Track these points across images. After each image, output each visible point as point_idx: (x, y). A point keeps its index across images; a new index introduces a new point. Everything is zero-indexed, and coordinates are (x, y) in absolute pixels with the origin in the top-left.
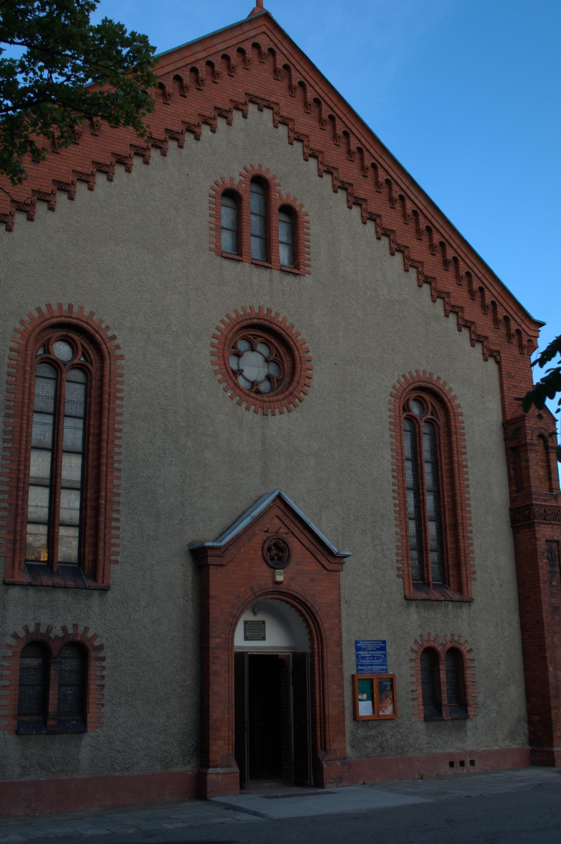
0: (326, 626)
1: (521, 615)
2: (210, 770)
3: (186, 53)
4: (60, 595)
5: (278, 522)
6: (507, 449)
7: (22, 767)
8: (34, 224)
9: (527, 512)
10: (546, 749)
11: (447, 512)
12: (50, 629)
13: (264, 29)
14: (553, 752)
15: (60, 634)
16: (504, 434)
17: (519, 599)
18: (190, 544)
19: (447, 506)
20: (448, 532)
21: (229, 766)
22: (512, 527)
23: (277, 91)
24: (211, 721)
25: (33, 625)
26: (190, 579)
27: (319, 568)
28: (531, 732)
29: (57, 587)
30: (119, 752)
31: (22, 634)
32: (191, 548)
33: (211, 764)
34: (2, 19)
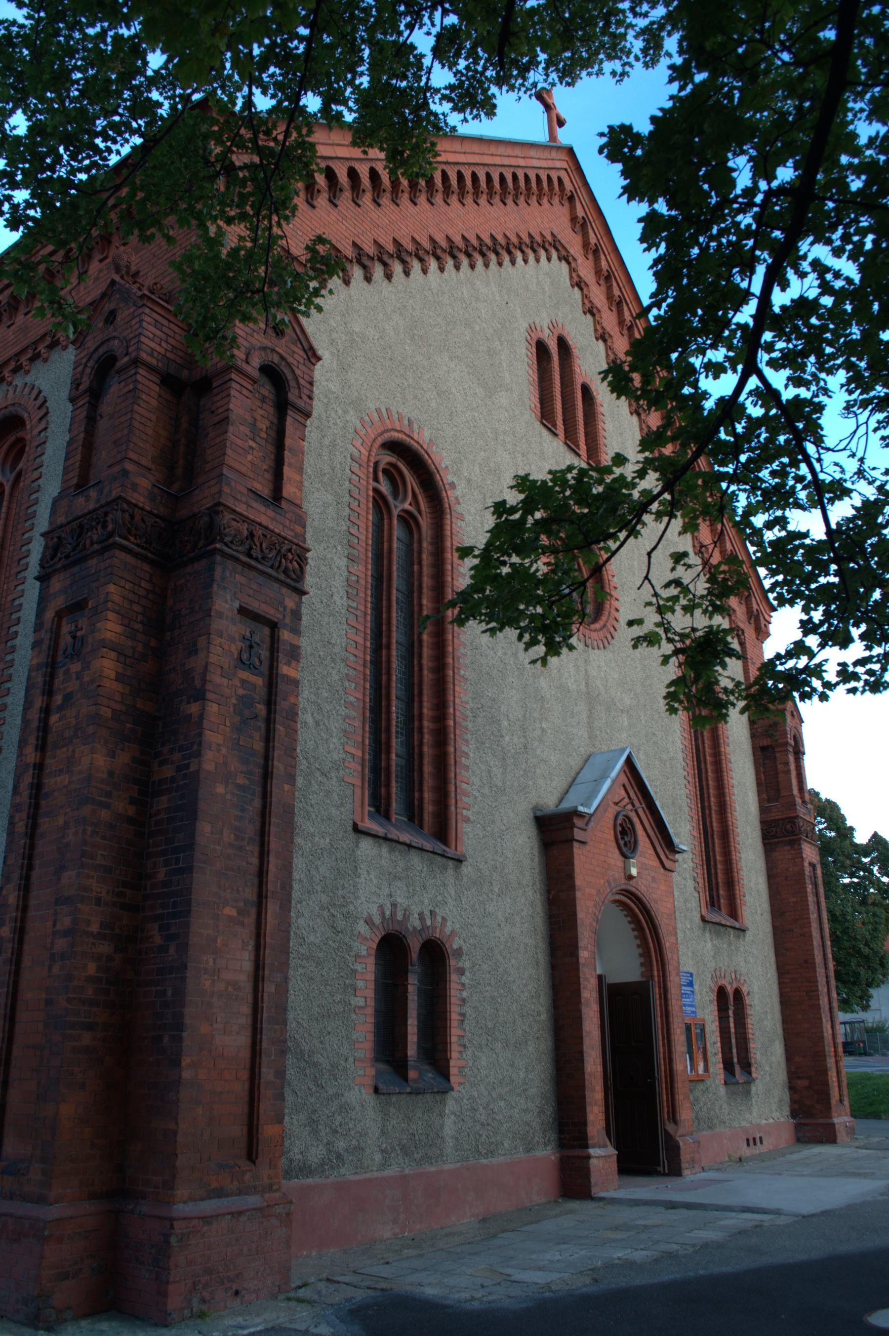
0: (668, 945)
1: (778, 954)
2: (591, 1151)
3: (518, 152)
4: (415, 859)
5: (623, 793)
6: (754, 748)
7: (382, 1151)
8: (371, 288)
9: (789, 827)
10: (821, 1121)
11: (714, 816)
12: (407, 914)
13: (566, 166)
14: (833, 1125)
15: (417, 924)
16: (751, 729)
17: (775, 934)
18: (535, 808)
19: (713, 808)
20: (716, 841)
21: (605, 1146)
22: (764, 844)
23: (573, 243)
24: (587, 1077)
25: (389, 905)
26: (536, 860)
27: (657, 863)
28: (793, 1102)
29: (415, 847)
30: (483, 1125)
31: (377, 920)
32: (539, 814)
33: (590, 1142)
34: (528, 5)
